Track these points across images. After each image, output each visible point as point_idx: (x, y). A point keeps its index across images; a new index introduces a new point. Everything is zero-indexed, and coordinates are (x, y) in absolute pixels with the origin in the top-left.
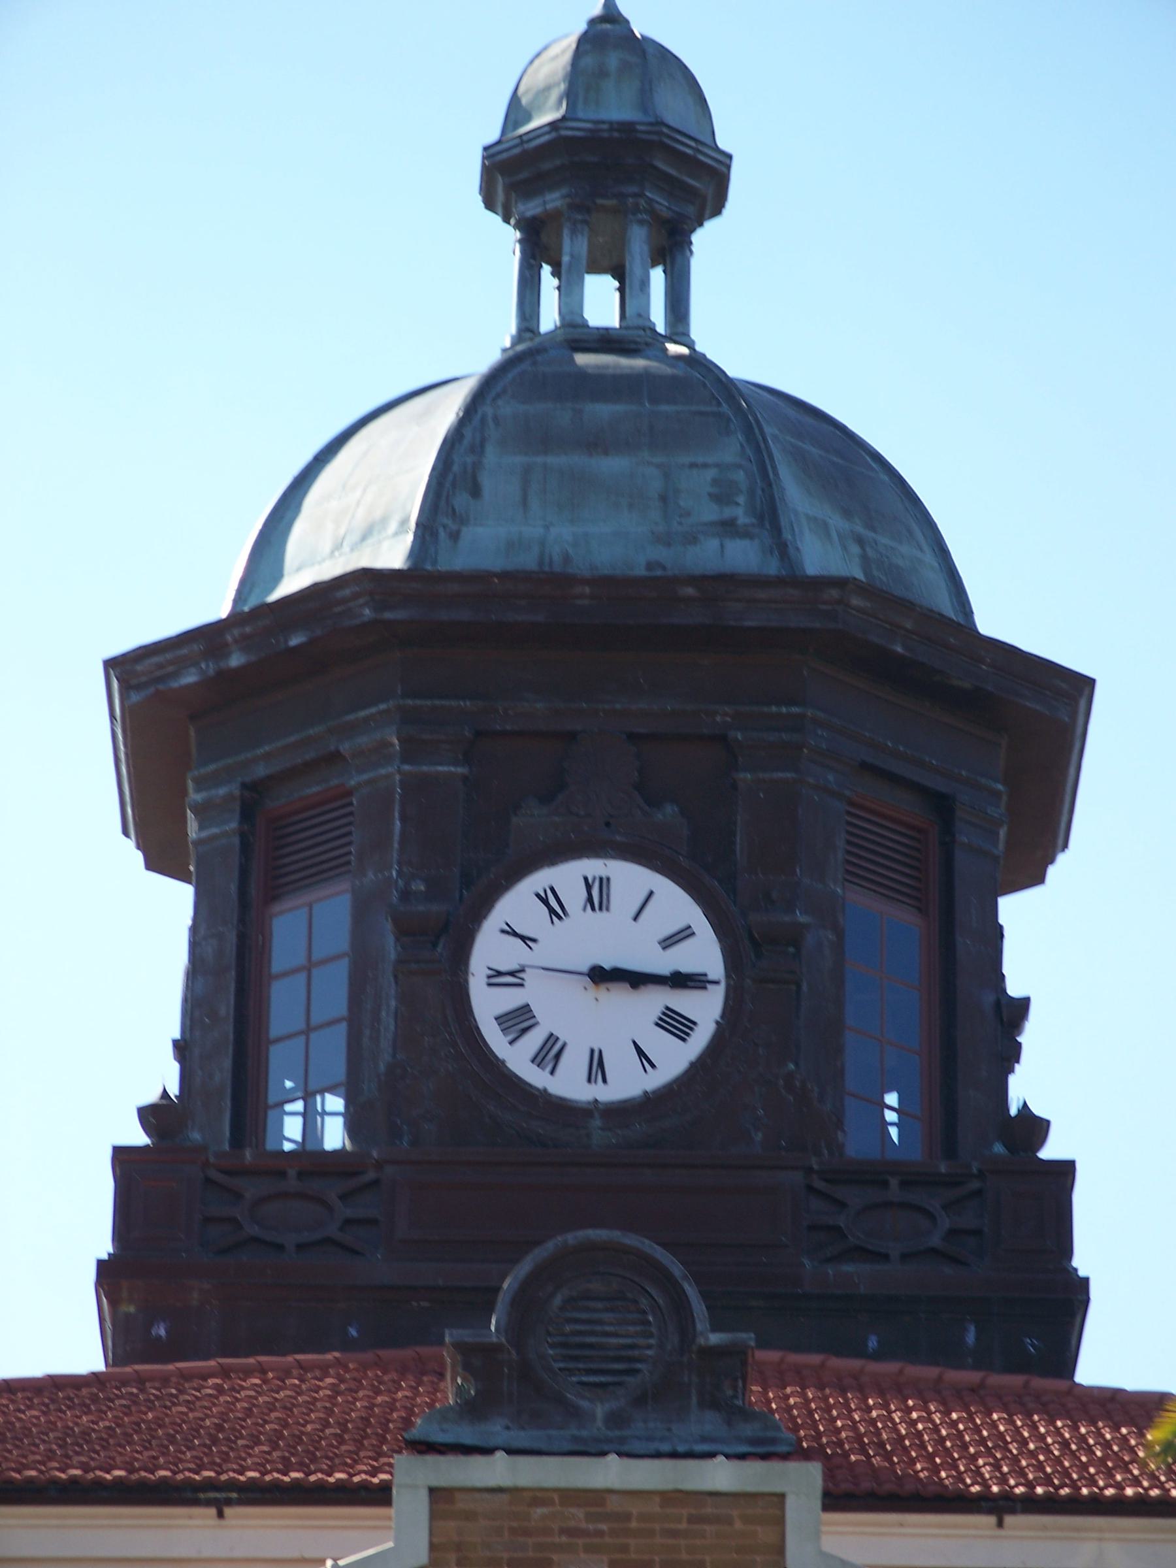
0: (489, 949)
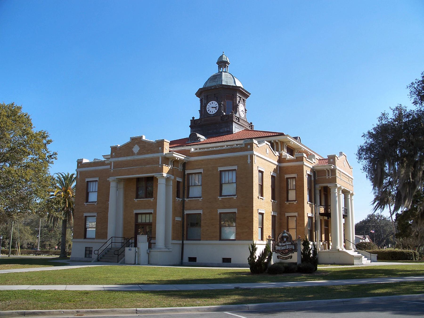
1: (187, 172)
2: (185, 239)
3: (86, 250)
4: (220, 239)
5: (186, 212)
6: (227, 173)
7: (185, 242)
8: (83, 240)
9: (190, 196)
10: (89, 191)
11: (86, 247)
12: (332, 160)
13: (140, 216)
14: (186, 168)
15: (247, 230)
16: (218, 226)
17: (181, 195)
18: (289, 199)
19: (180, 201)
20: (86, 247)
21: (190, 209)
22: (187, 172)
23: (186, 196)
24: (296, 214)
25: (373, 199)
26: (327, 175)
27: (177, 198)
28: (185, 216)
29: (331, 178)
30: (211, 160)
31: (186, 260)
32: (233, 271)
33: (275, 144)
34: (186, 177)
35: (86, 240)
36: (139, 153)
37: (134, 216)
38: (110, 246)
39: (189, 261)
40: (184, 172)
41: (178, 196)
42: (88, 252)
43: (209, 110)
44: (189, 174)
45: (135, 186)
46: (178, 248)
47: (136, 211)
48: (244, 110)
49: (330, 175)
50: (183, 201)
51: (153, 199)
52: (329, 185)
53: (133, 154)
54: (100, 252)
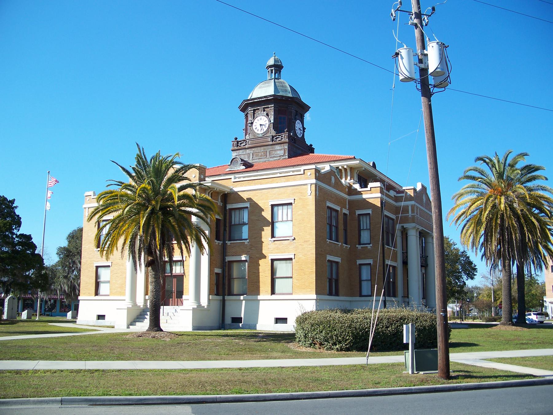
0: (254, 124)
1: (229, 206)
4: (361, 296)
6: (280, 208)
8: (358, 298)
10: (275, 220)
17: (222, 237)
18: (362, 242)
19: (220, 244)
22: (229, 206)
24: (371, 261)
25: (99, 255)
27: (216, 241)
31: (228, 321)
32: (466, 348)
33: (343, 171)
34: (228, 212)
35: (274, 297)
40: (225, 207)
41: (218, 238)
44: (231, 210)
46: (216, 305)
48: (302, 129)
50: (224, 245)
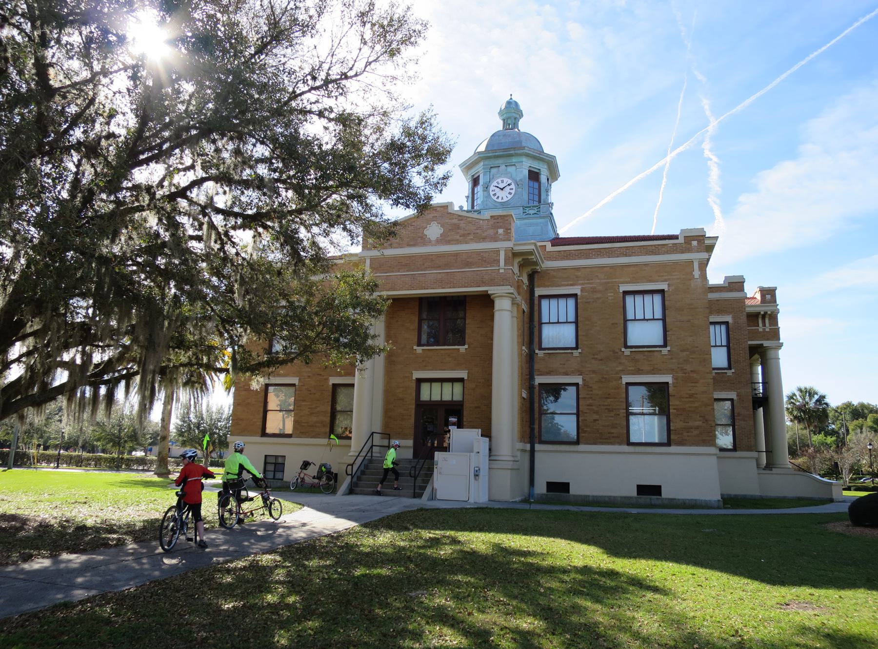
2: (537, 440)
3: (266, 463)
5: (539, 380)
7: (538, 447)
9: (543, 346)
11: (266, 456)
12: (768, 297)
13: (425, 387)
14: (536, 284)
15: (697, 423)
16: (623, 412)
20: (266, 456)
21: (549, 373)
23: (536, 345)
26: (761, 324)
28: (537, 390)
29: (767, 330)
30: (601, 267)
35: (265, 439)
36: (444, 240)
37: (414, 385)
38: (369, 454)
39: (638, 494)
42: (271, 468)
43: (495, 195)
45: (416, 319)
47: (417, 375)
49: (767, 325)
51: (466, 346)
52: (766, 343)
53: (423, 240)
54: (355, 468)
